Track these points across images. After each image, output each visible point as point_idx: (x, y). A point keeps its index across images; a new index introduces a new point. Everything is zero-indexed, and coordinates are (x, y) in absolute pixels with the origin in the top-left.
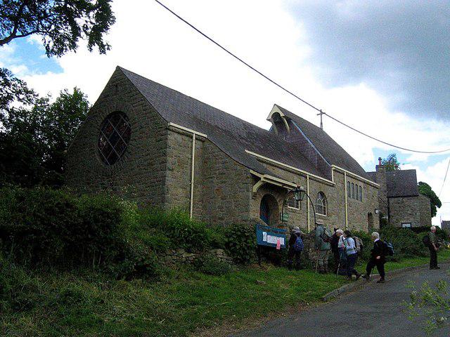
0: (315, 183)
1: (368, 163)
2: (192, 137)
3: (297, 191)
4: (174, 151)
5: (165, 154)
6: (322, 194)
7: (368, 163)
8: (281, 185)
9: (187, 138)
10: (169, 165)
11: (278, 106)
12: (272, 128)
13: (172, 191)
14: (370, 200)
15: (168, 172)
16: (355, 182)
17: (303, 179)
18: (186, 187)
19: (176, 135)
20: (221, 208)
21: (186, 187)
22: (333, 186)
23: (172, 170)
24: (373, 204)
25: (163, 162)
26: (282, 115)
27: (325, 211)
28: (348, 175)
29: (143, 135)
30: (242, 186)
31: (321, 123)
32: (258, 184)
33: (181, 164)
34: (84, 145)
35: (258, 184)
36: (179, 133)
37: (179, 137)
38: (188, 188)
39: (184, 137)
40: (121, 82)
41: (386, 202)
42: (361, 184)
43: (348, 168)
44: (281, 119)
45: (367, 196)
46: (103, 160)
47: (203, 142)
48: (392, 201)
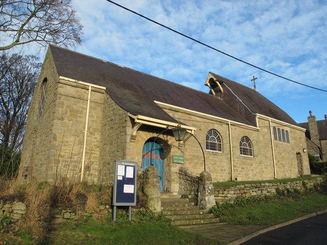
8: (165, 127)
22: (258, 131)
26: (215, 79)
31: (255, 86)
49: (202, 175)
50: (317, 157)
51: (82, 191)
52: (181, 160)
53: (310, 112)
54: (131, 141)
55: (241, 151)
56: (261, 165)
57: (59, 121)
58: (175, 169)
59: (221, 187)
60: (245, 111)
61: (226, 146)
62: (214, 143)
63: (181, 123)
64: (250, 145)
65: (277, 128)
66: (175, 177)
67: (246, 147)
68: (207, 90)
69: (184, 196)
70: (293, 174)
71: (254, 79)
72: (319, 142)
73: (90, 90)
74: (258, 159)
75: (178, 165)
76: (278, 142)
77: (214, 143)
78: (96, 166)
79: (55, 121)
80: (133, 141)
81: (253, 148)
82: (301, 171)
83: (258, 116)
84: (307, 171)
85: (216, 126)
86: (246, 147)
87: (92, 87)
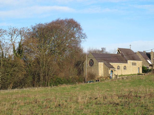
58: (114, 74)
59: (119, 76)
61: (121, 68)
62: (119, 68)
64: (126, 67)
66: (114, 75)
67: (125, 68)
69: (115, 77)
70: (137, 72)
71: (130, 46)
77: (119, 68)
78: (103, 74)
82: (139, 72)
84: (141, 72)
85: (119, 65)
86: (125, 68)
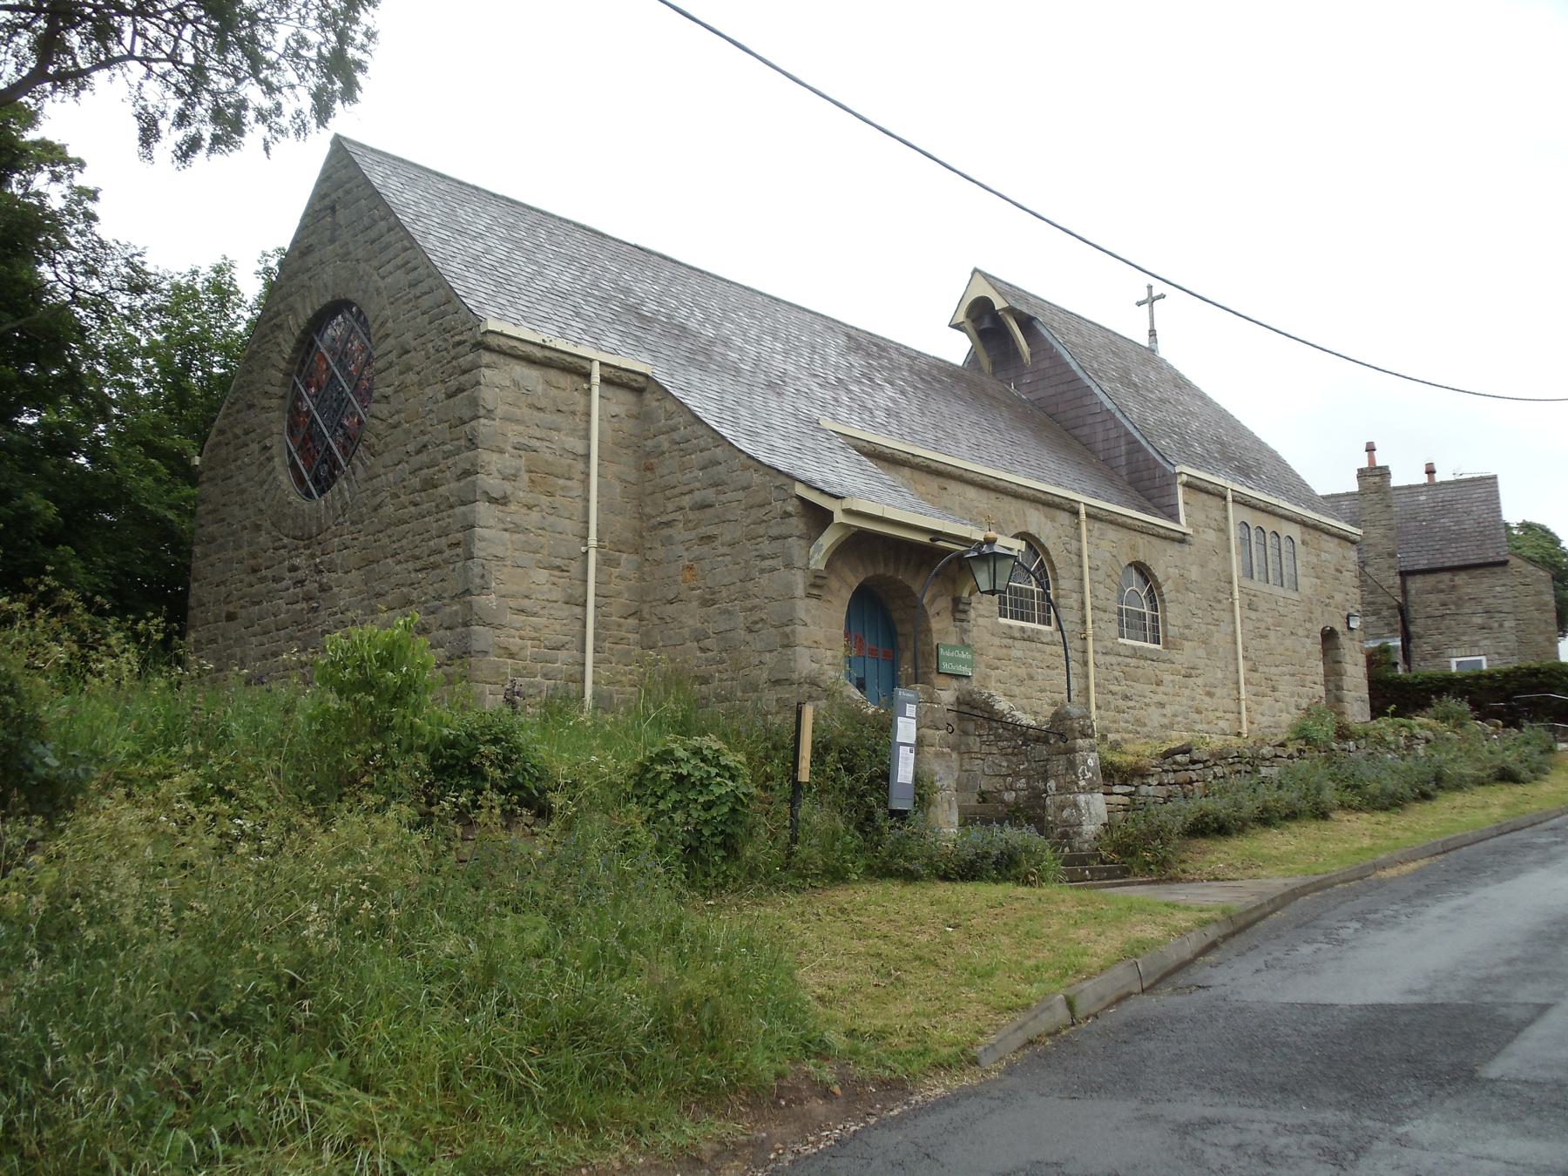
0: (1112, 534)
1: (1354, 486)
2: (587, 376)
3: (983, 558)
4: (512, 430)
5: (472, 443)
6: (1142, 569)
7: (1354, 486)
8: (925, 539)
9: (565, 381)
10: (490, 481)
11: (986, 276)
12: (972, 359)
13: (503, 580)
14: (1326, 587)
15: (483, 509)
16: (1269, 524)
17: (1064, 517)
18: (567, 566)
19: (972, 493)
20: (699, 636)
21: (567, 566)
22: (1182, 539)
23: (502, 501)
24: (1339, 597)
25: (466, 473)
26: (999, 304)
27: (1155, 629)
28: (1243, 502)
29: (411, 377)
30: (766, 547)
31: (1152, 333)
32: (828, 539)
33: (542, 476)
34: (247, 433)
35: (828, 539)
36: (530, 361)
37: (532, 377)
38: (575, 567)
39: (554, 375)
40: (349, 200)
41: (1396, 591)
42: (1295, 531)
43: (1244, 471)
44: (996, 323)
45: (1317, 571)
46: (300, 480)
47: (639, 391)
48: (1415, 584)
49: (1059, 717)
50: (1395, 648)
51: (1373, 644)
52: (963, 662)
53: (1370, 449)
54: (809, 595)
55: (1121, 623)
56: (1191, 681)
57: (495, 510)
60: (1128, 453)
63: (290, 453)
65: (1268, 530)
68: (956, 348)
72: (1398, 580)
73: (596, 378)
74: (1183, 657)
75: (954, 683)
76: (1256, 585)
79: (483, 509)
80: (815, 592)
81: (1164, 611)
83: (1185, 478)
84: (1357, 710)
87: (602, 364)
